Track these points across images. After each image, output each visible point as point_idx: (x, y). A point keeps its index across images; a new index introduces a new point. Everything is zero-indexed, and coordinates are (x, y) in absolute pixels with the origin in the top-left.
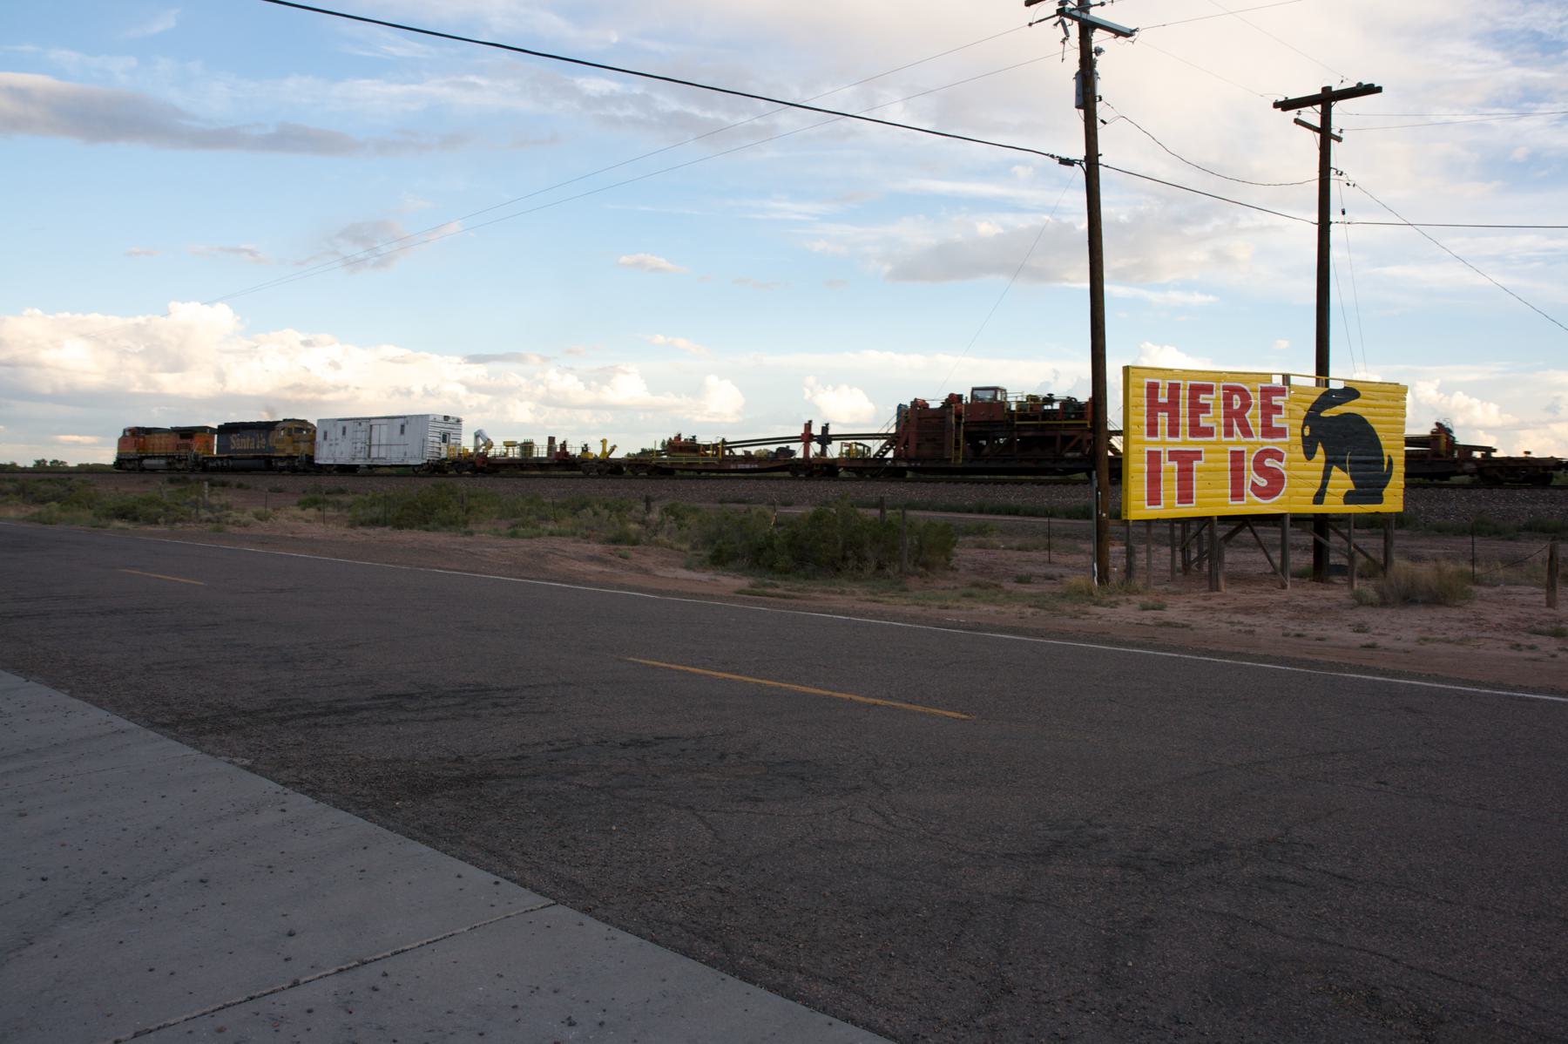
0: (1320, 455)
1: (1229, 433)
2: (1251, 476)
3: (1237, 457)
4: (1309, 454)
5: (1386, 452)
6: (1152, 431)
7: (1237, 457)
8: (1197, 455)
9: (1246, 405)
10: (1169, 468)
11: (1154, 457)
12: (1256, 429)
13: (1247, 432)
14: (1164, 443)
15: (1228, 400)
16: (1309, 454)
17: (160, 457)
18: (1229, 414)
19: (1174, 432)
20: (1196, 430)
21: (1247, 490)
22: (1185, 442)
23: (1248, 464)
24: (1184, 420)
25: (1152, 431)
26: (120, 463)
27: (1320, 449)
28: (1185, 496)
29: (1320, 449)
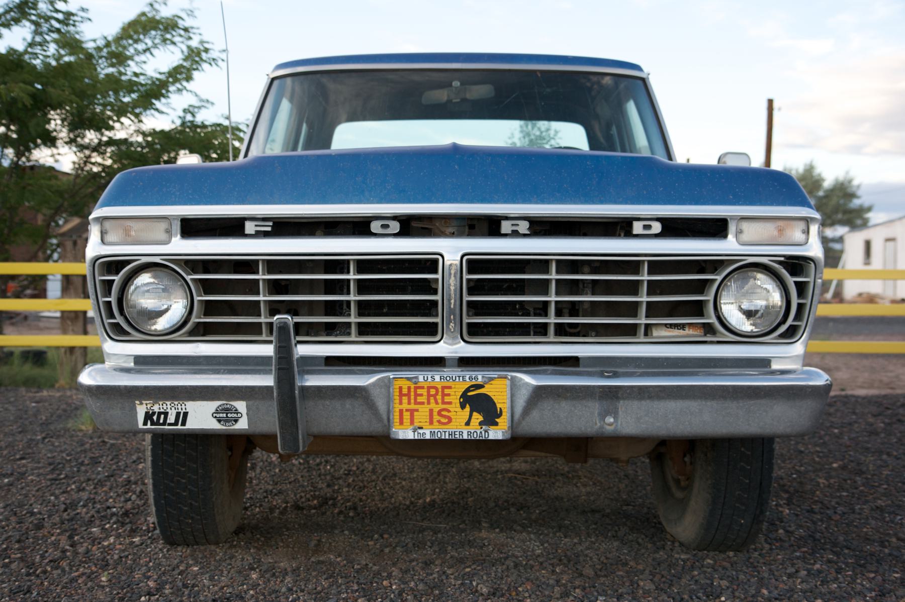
0: (468, 408)
1: (429, 403)
2: (436, 417)
3: (431, 411)
4: (463, 407)
5: (499, 406)
6: (401, 403)
7: (431, 411)
8: (417, 410)
9: (437, 393)
10: (407, 415)
11: (401, 411)
12: (440, 401)
13: (437, 403)
14: (405, 406)
15: (428, 392)
16: (463, 407)
17: (56, 311)
18: (429, 395)
19: (409, 403)
20: (416, 403)
21: (435, 420)
22: (413, 406)
23: (435, 414)
24: (412, 401)
25: (401, 403)
26: (370, 222)
27: (468, 406)
28: (184, 424)
29: (468, 406)
